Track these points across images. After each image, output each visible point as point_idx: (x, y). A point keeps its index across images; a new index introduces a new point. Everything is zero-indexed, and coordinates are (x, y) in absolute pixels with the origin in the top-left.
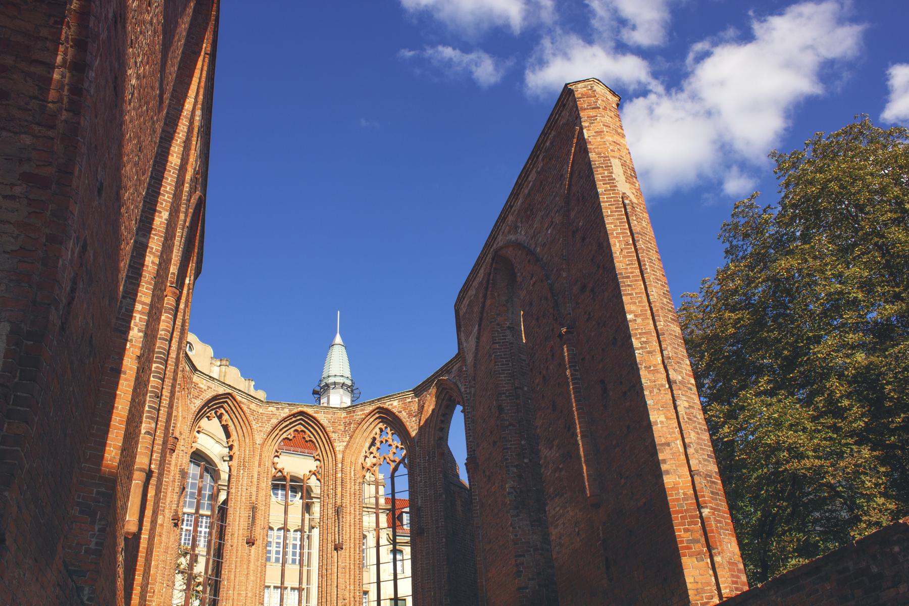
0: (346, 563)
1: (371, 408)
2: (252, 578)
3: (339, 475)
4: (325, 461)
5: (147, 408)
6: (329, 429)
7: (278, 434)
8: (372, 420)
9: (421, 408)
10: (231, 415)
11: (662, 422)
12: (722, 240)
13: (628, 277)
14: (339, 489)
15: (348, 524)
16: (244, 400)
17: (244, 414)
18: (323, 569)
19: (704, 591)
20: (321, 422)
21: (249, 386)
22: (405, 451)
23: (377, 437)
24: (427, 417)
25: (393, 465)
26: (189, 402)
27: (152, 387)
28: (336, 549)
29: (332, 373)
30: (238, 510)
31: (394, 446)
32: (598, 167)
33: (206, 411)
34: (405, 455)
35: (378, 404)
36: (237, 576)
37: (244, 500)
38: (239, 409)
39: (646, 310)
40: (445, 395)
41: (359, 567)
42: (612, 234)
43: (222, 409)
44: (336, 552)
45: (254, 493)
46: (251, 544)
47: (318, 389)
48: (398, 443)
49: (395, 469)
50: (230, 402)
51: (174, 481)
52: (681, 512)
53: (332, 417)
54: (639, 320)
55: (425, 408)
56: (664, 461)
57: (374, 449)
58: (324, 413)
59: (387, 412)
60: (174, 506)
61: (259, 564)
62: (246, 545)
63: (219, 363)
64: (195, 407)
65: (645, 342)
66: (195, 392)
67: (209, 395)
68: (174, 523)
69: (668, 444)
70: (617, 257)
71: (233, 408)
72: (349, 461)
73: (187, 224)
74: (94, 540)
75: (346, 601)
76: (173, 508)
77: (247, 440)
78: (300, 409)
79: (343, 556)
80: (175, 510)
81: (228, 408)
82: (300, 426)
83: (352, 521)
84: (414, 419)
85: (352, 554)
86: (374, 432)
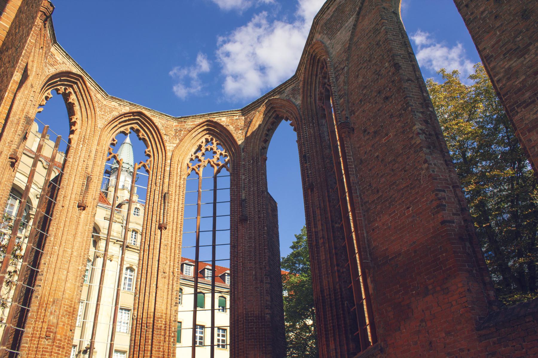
0: (168, 241)
1: (201, 121)
2: (79, 239)
3: (168, 169)
4: (156, 157)
6: (163, 132)
7: (116, 126)
9: (248, 124)
10: (78, 96)
14: (167, 180)
15: (172, 210)
16: (92, 88)
17: (91, 99)
18: (146, 244)
20: (156, 124)
22: (229, 158)
23: (203, 145)
24: (254, 130)
25: (216, 168)
31: (218, 153)
33: (56, 82)
34: (229, 160)
35: (208, 118)
36: (65, 234)
37: (80, 170)
38: (87, 93)
40: (273, 113)
41: (179, 247)
43: (71, 89)
44: (159, 230)
45: (90, 166)
46: (82, 208)
48: (221, 151)
50: (80, 85)
51: (18, 124)
53: (165, 123)
55: (253, 122)
57: (199, 154)
58: (159, 119)
59: (217, 125)
61: (87, 229)
62: (77, 209)
64: (49, 72)
68: (11, 162)
71: (82, 91)
72: (177, 159)
75: (166, 274)
76: (12, 148)
77: (90, 122)
78: (139, 110)
79: (166, 235)
80: (15, 150)
81: (77, 90)
82: (136, 125)
83: (176, 208)
84: (240, 131)
86: (201, 141)
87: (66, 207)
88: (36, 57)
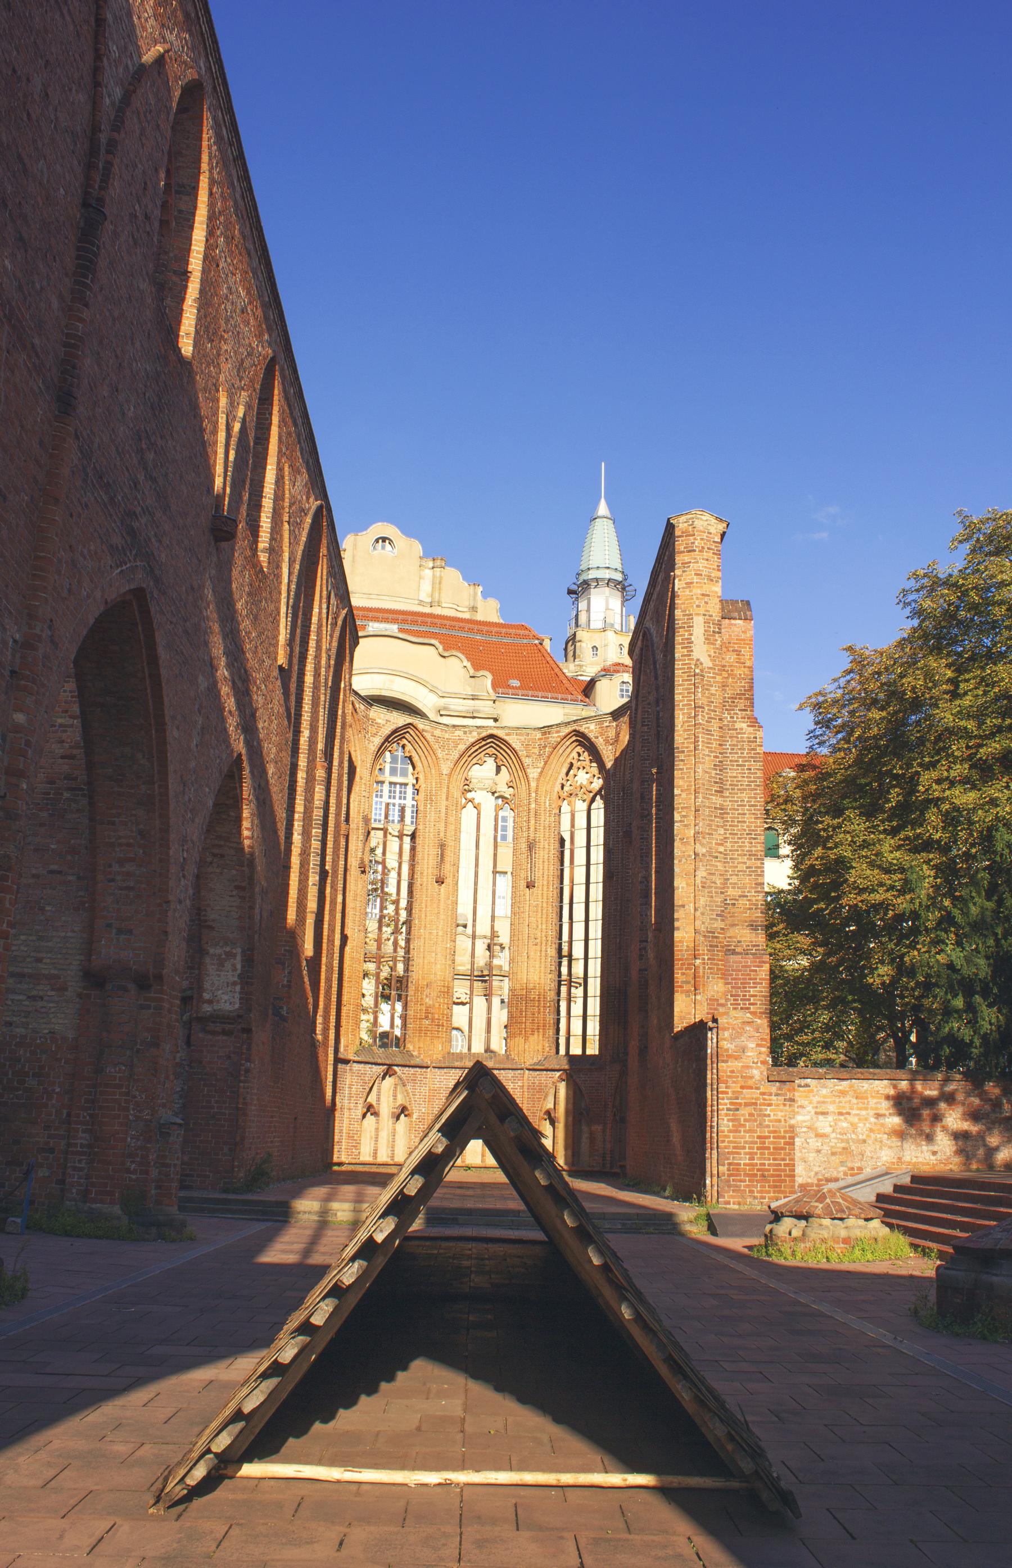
2: (442, 917)
3: (533, 806)
5: (311, 866)
8: (568, 743)
11: (683, 888)
12: (901, 605)
13: (683, 752)
14: (533, 822)
15: (541, 860)
19: (685, 1018)
20: (514, 745)
21: (475, 594)
23: (574, 762)
26: (367, 742)
27: (314, 848)
28: (528, 886)
29: (593, 564)
30: (426, 847)
32: (680, 628)
35: (575, 727)
39: (691, 786)
42: (679, 705)
45: (442, 829)
47: (574, 587)
49: (593, 800)
50: (412, 732)
52: (682, 960)
54: (684, 795)
56: (678, 919)
59: (583, 735)
60: (360, 854)
63: (431, 564)
65: (684, 816)
66: (372, 730)
67: (387, 731)
69: (683, 906)
70: (678, 731)
73: (330, 684)
74: (286, 979)
75: (538, 941)
77: (433, 771)
84: (610, 747)
85: (545, 892)
86: (571, 756)
87: (424, 884)
88: (357, 745)
